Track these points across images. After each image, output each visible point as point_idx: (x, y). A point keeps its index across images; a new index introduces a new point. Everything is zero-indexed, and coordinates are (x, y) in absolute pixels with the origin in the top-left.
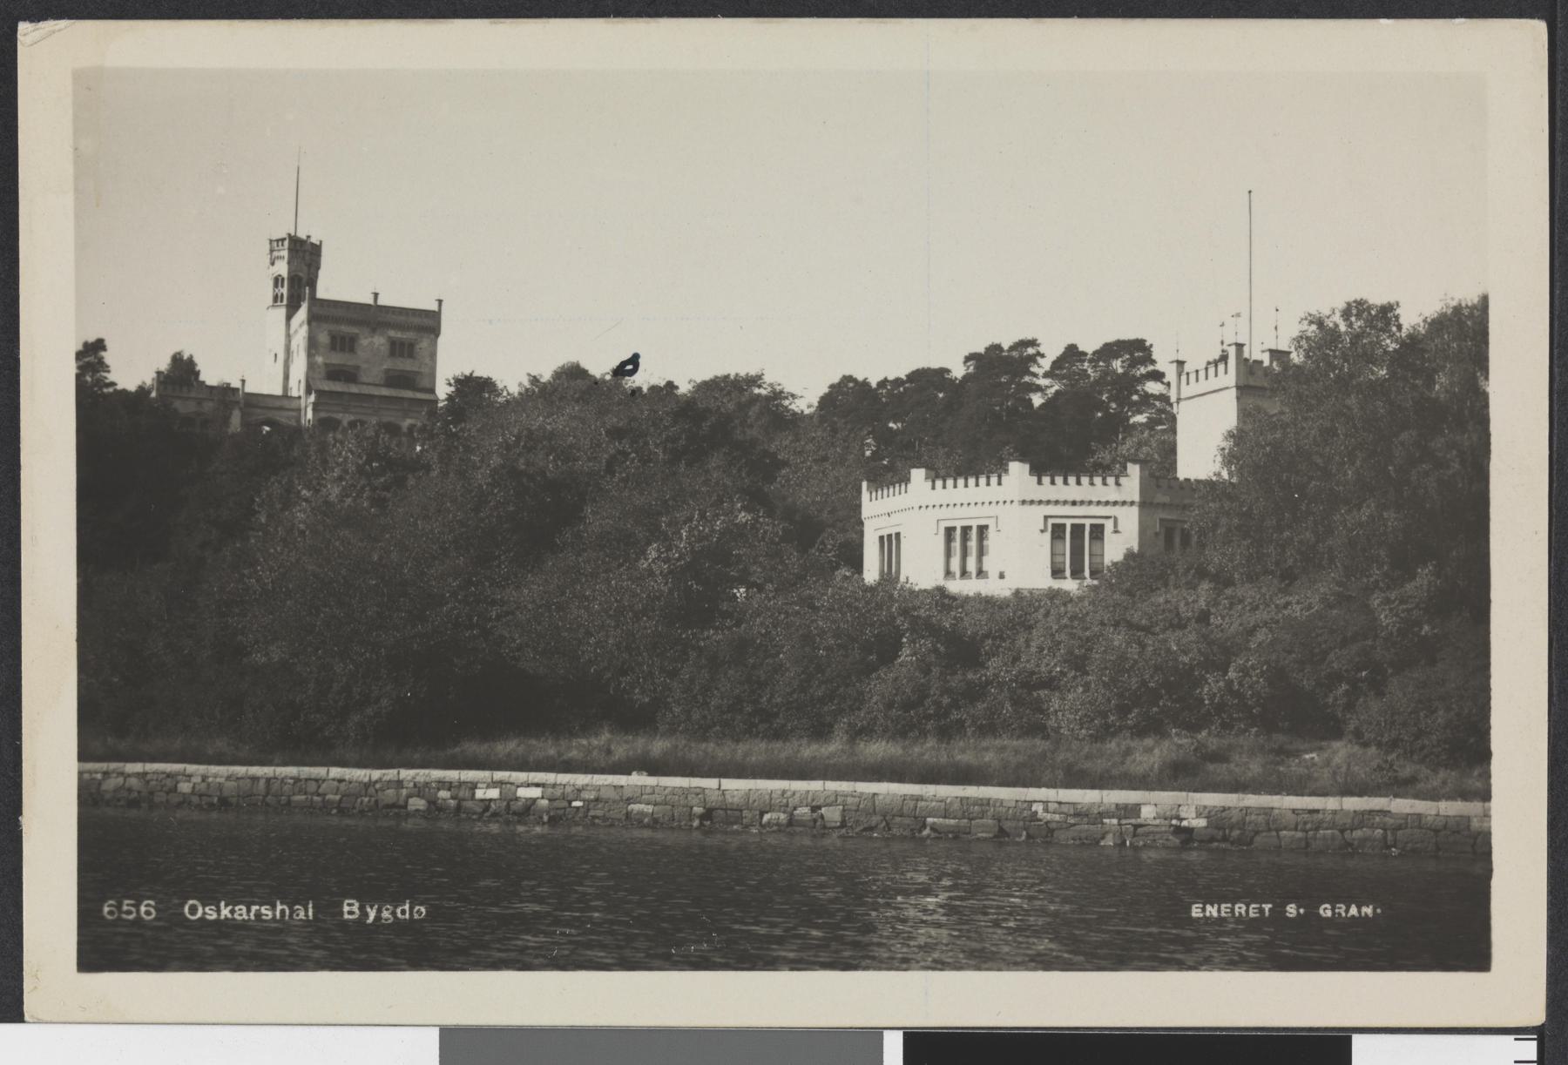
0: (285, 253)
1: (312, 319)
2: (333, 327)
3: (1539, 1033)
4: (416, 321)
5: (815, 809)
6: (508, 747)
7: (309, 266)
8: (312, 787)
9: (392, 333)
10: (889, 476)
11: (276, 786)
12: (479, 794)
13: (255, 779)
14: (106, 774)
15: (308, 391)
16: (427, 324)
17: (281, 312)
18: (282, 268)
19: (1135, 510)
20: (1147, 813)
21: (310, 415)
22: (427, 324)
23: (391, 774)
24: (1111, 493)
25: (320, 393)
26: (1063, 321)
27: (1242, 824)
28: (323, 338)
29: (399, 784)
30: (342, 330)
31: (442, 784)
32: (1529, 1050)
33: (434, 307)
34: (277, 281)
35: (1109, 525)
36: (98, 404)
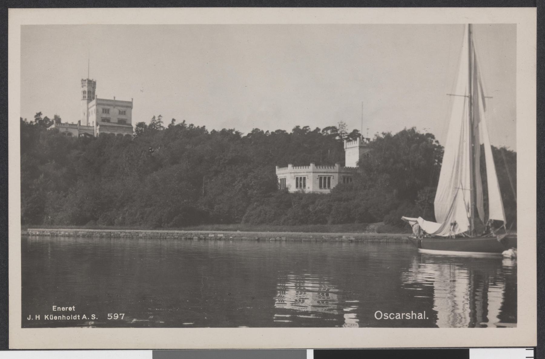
0: (86, 84)
1: (98, 104)
2: (103, 107)
3: (535, 349)
4: (126, 104)
5: (280, 237)
6: (216, 226)
7: (93, 88)
8: (171, 235)
9: (119, 108)
10: (284, 165)
11: (163, 235)
12: (209, 236)
13: (157, 233)
14: (121, 232)
15: (97, 124)
16: (129, 105)
17: (86, 102)
18: (86, 89)
19: (337, 174)
20: (344, 237)
21: (98, 132)
22: (129, 105)
23: (189, 232)
24: (333, 170)
25: (101, 126)
26: (317, 121)
27: (361, 239)
28: (101, 110)
29: (192, 234)
30: (105, 106)
31: (201, 234)
32: (531, 353)
33: (131, 100)
34: (84, 92)
35: (332, 177)
36: (24, 126)
